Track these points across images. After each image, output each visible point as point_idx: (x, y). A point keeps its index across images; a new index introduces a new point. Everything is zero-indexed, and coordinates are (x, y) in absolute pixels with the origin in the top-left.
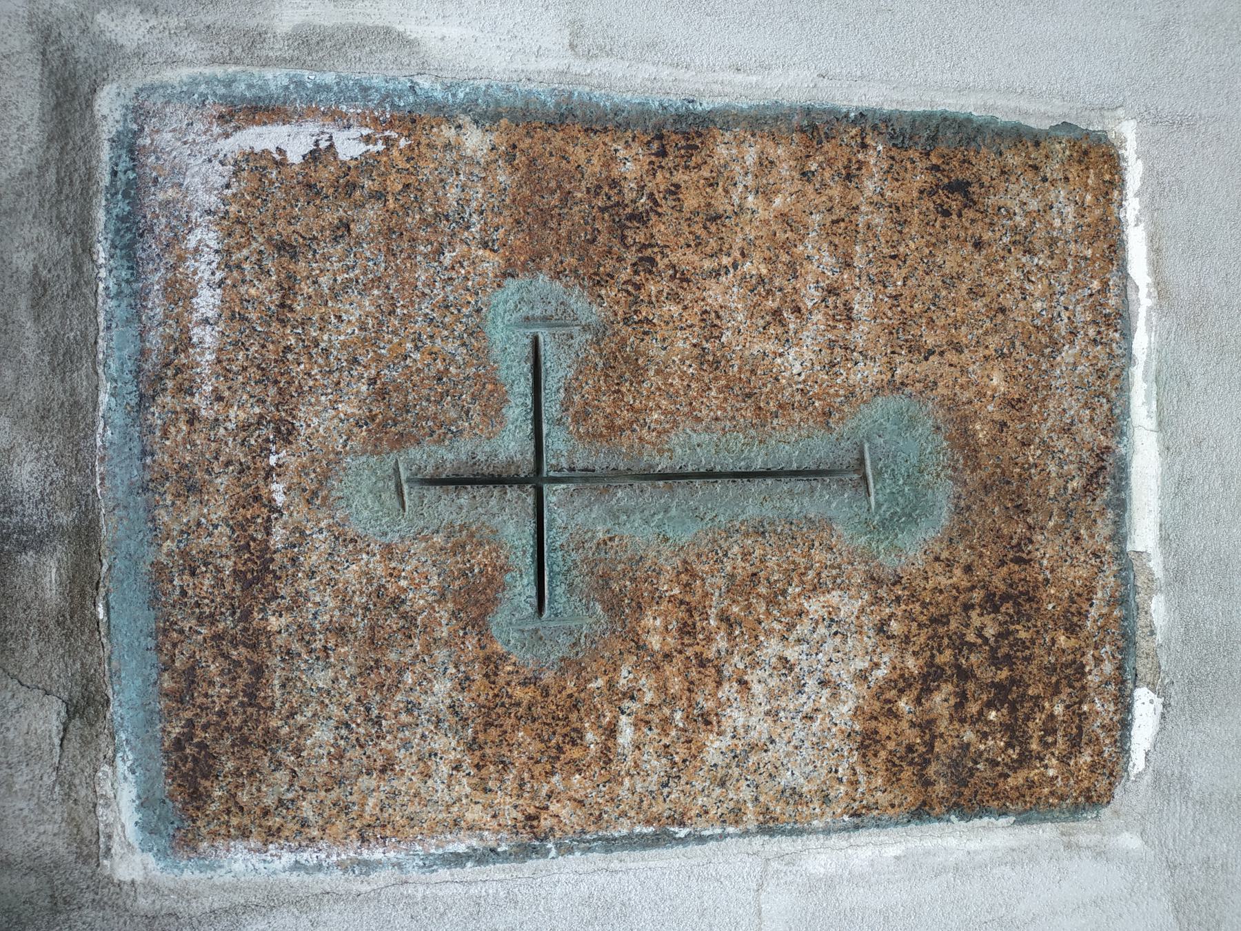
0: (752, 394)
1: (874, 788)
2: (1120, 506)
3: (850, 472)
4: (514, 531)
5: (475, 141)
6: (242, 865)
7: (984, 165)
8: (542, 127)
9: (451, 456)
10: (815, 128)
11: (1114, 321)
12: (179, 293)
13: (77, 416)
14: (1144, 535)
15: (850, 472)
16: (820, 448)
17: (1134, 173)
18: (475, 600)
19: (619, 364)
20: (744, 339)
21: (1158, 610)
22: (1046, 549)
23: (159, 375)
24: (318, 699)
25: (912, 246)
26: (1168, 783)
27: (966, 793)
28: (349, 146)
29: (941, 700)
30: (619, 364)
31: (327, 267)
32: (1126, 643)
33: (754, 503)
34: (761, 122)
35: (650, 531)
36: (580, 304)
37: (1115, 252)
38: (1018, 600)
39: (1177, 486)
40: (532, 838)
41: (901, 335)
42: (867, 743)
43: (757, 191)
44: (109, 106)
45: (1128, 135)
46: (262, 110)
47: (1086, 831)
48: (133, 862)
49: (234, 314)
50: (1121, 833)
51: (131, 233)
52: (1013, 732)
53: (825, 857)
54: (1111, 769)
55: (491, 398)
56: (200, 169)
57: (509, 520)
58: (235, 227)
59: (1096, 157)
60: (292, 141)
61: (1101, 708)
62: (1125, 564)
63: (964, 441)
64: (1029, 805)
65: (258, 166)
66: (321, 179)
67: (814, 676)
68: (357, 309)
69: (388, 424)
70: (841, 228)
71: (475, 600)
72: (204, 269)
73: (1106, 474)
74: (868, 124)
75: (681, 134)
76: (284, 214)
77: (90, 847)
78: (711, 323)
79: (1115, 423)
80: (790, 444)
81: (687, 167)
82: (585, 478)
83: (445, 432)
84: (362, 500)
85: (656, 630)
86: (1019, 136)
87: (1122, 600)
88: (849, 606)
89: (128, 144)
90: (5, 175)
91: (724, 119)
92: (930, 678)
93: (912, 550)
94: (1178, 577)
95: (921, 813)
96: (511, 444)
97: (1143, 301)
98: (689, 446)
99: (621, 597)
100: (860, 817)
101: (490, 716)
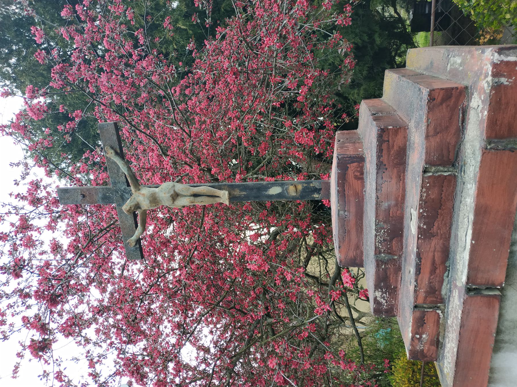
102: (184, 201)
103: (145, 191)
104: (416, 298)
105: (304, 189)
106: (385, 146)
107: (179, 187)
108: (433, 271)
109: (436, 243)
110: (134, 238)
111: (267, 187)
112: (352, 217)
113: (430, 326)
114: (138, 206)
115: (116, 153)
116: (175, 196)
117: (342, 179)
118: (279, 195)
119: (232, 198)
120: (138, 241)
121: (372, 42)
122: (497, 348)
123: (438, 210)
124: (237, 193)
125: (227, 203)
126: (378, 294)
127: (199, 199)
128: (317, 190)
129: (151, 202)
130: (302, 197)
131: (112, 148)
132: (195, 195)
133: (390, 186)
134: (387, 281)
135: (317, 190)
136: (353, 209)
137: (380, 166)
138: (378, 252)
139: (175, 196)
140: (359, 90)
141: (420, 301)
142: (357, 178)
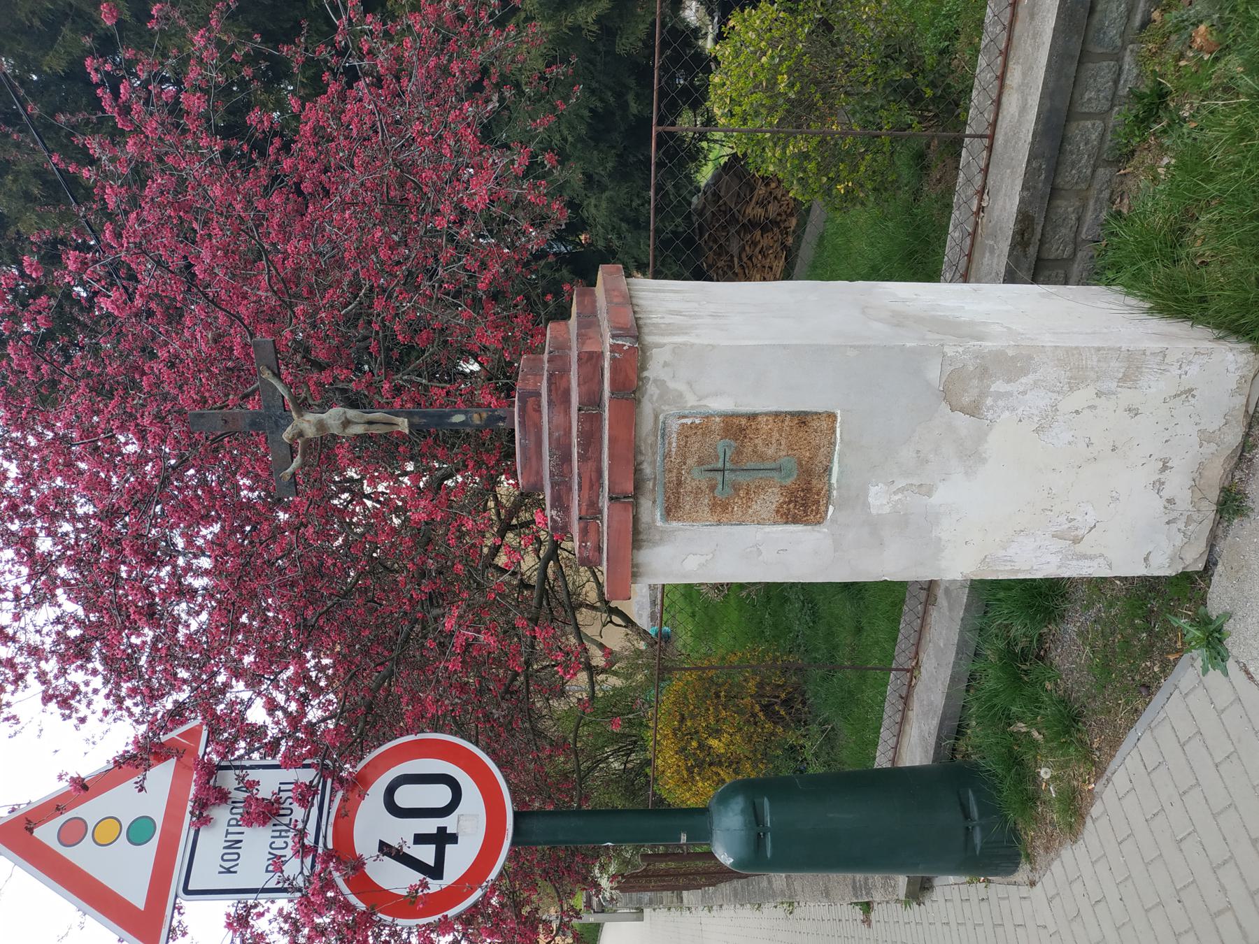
0: (762, 457)
1: (778, 518)
2: (830, 475)
3: (779, 469)
4: (720, 478)
5: (718, 419)
6: (674, 524)
7: (809, 418)
8: (728, 417)
9: (710, 467)
10: (777, 414)
11: (834, 444)
12: (670, 443)
13: (655, 461)
14: (834, 480)
15: (779, 469)
16: (773, 465)
17: (839, 419)
18: (712, 488)
19: (739, 452)
20: (761, 448)
21: (835, 493)
22: (814, 482)
23: (666, 456)
24: (687, 502)
25: (794, 432)
26: (833, 521)
27: (796, 520)
28: (697, 421)
29: (791, 506)
30: (739, 452)
31: (693, 439)
32: (829, 497)
33: (760, 474)
34: (766, 414)
35: (742, 478)
36: (732, 443)
37: (834, 432)
38: (809, 490)
39: (841, 473)
40: (719, 523)
41: (790, 447)
42: (777, 512)
43: (764, 425)
44: (661, 418)
45: (839, 413)
46: (684, 417)
47: (817, 528)
48: (659, 523)
49: (678, 447)
50: (824, 529)
51: (663, 436)
52: (805, 511)
53: (767, 529)
54: (823, 518)
55: (717, 458)
56: (674, 425)
57: (719, 476)
58: (679, 434)
59: (832, 416)
60: (688, 421)
61: (822, 508)
62: (830, 485)
63: (800, 464)
64: (807, 523)
65: (683, 424)
66: (693, 426)
67: (772, 499)
68: (697, 445)
69: (701, 462)
70: (780, 430)
71: (712, 488)
72: (674, 440)
73: (828, 470)
74: (787, 413)
75: (753, 417)
76: (687, 433)
77: (654, 521)
78: (755, 446)
79: (831, 461)
80: (768, 465)
81: (514, 628)
82: (732, 470)
83: (709, 463)
84: (696, 473)
85: (742, 493)
86: (816, 413)
87: (829, 491)
88: (776, 490)
89: (664, 423)
90: (692, 13)
91: (761, 414)
92: (790, 502)
93: (788, 482)
94: (839, 488)
95: (786, 523)
96: (720, 465)
97: (838, 441)
98: (750, 465)
99: (736, 488)
100: (775, 523)
101: (714, 505)
102: (359, 429)
103: (310, 417)
104: (580, 511)
105: (489, 417)
106: (553, 387)
107: (352, 413)
108: (591, 488)
109: (591, 465)
110: (290, 470)
111: (450, 415)
112: (532, 445)
113: (592, 535)
114: (301, 434)
115: (274, 374)
116: (347, 423)
117: (523, 410)
118: (462, 423)
119: (411, 425)
120: (294, 475)
121: (624, 106)
122: (637, 543)
123: (590, 439)
124: (416, 420)
125: (407, 431)
126: (554, 513)
127: (374, 426)
128: (503, 419)
129: (318, 430)
130: (486, 425)
131: (269, 368)
132: (370, 423)
133: (559, 419)
134: (561, 503)
135: (503, 419)
136: (533, 438)
137: (550, 402)
138: (552, 475)
139: (347, 423)
140: (599, 199)
141: (583, 513)
142: (535, 410)
